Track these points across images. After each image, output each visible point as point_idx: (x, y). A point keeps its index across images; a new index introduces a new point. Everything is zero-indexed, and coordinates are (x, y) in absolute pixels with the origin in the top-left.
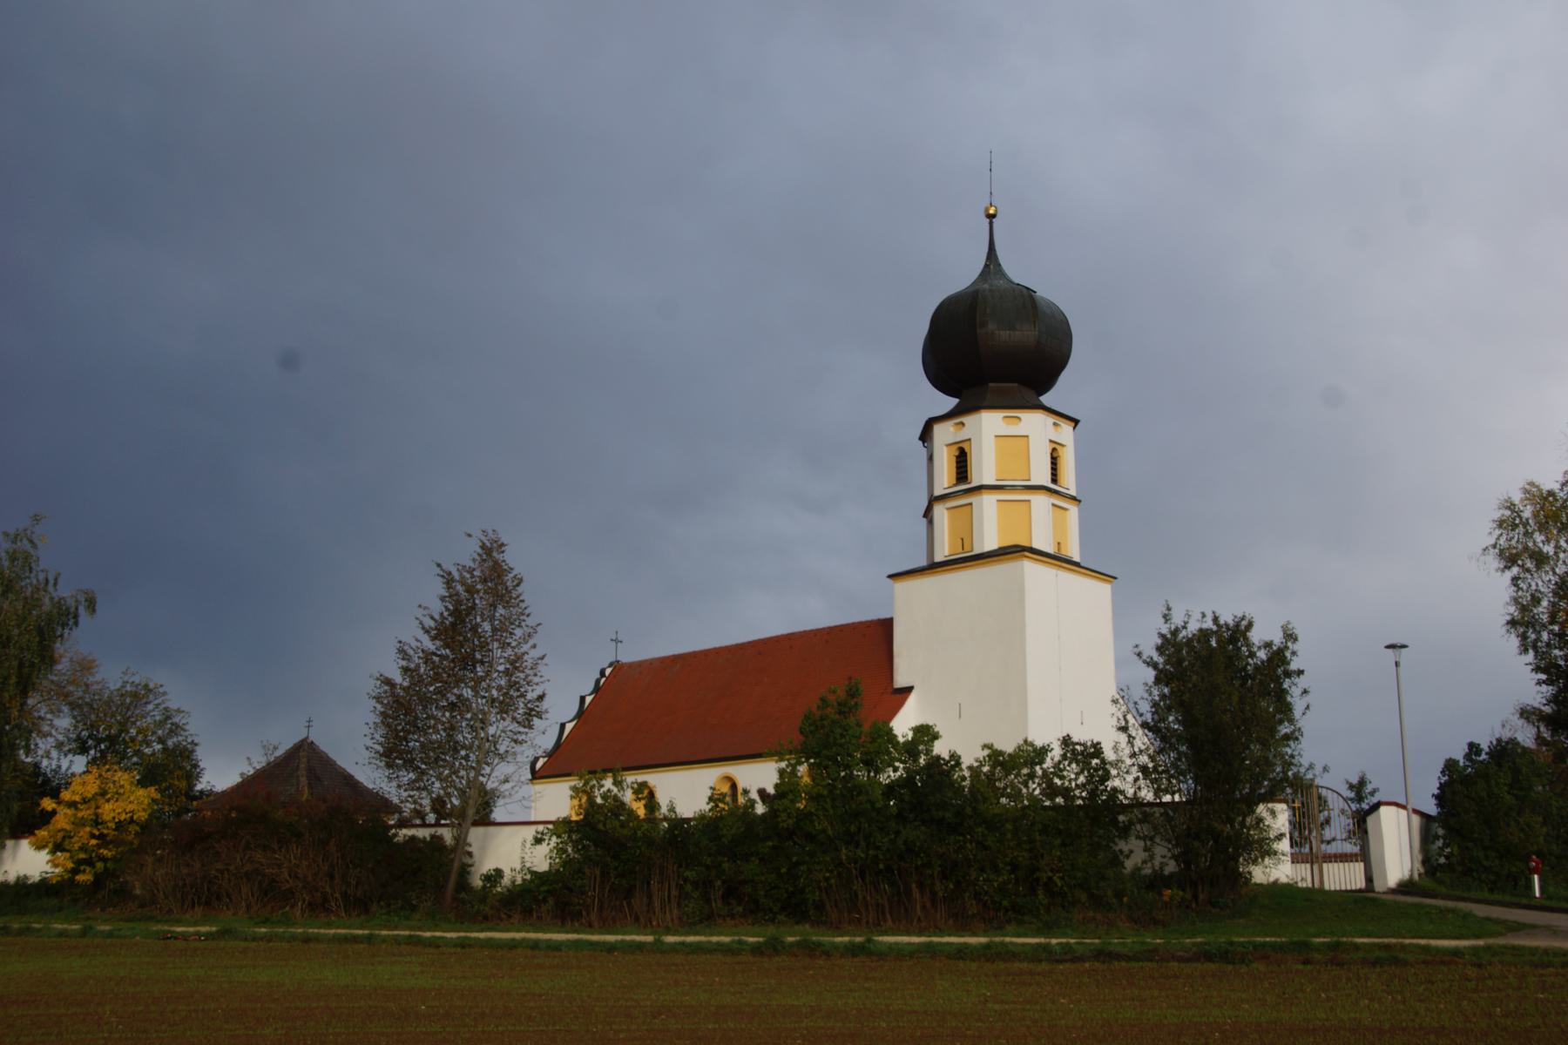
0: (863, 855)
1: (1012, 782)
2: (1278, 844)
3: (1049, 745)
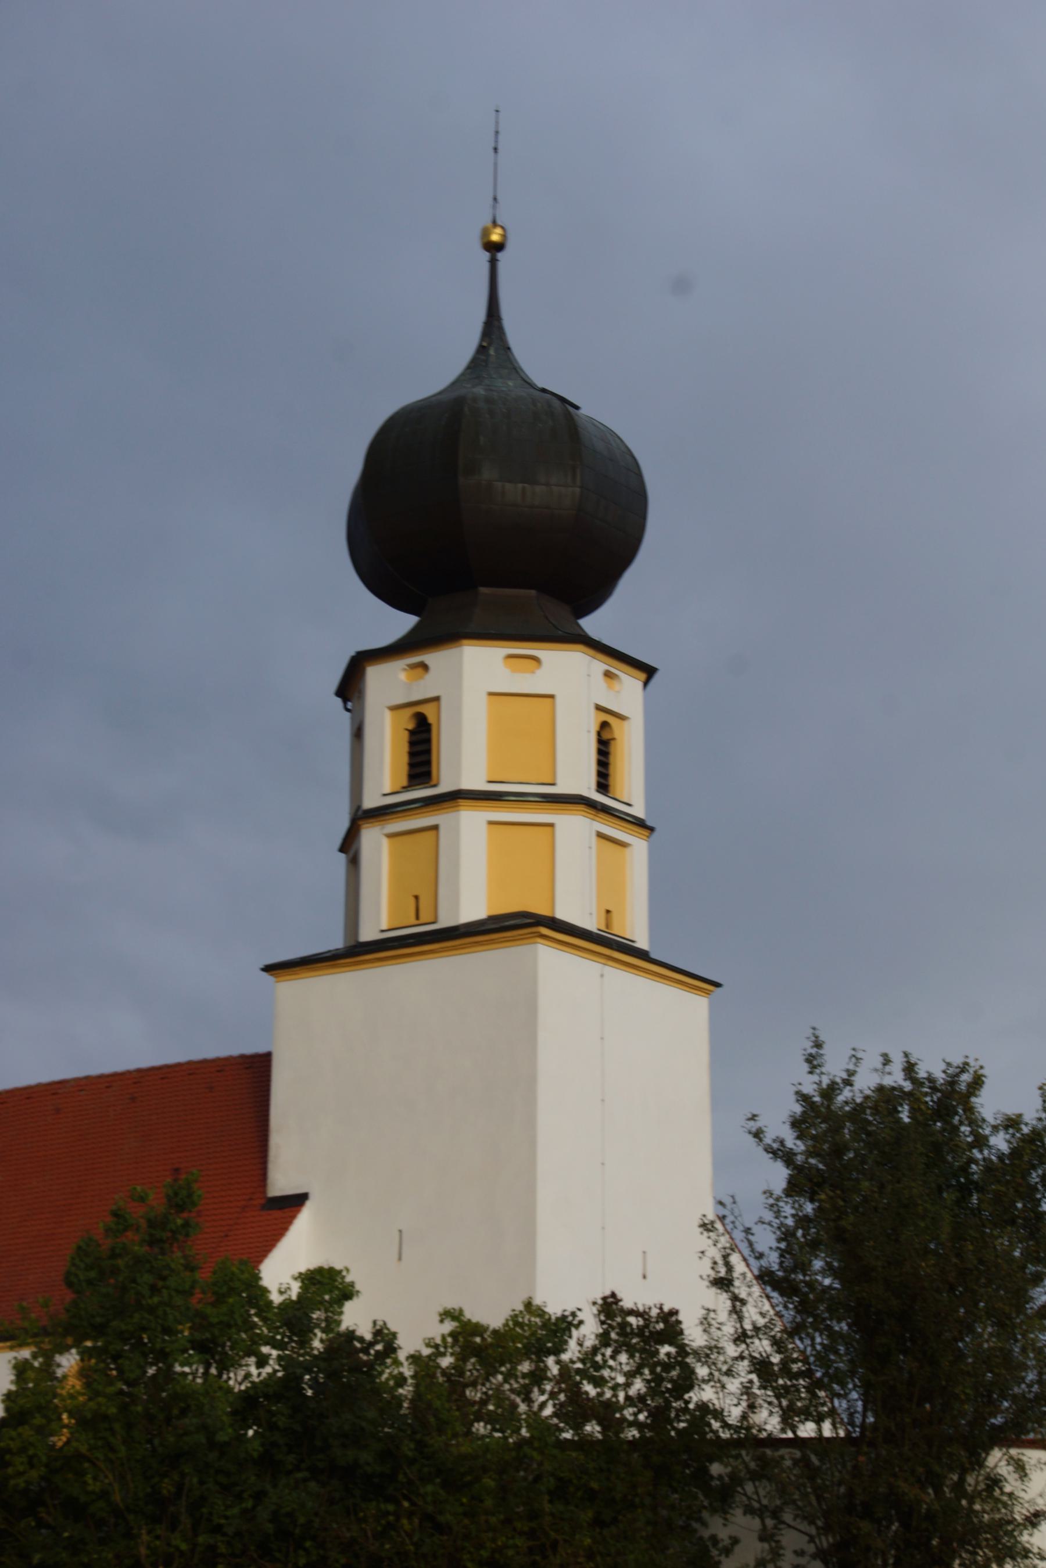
0: (184, 1547)
1: (498, 1389)
2: (1031, 1535)
3: (574, 1314)
